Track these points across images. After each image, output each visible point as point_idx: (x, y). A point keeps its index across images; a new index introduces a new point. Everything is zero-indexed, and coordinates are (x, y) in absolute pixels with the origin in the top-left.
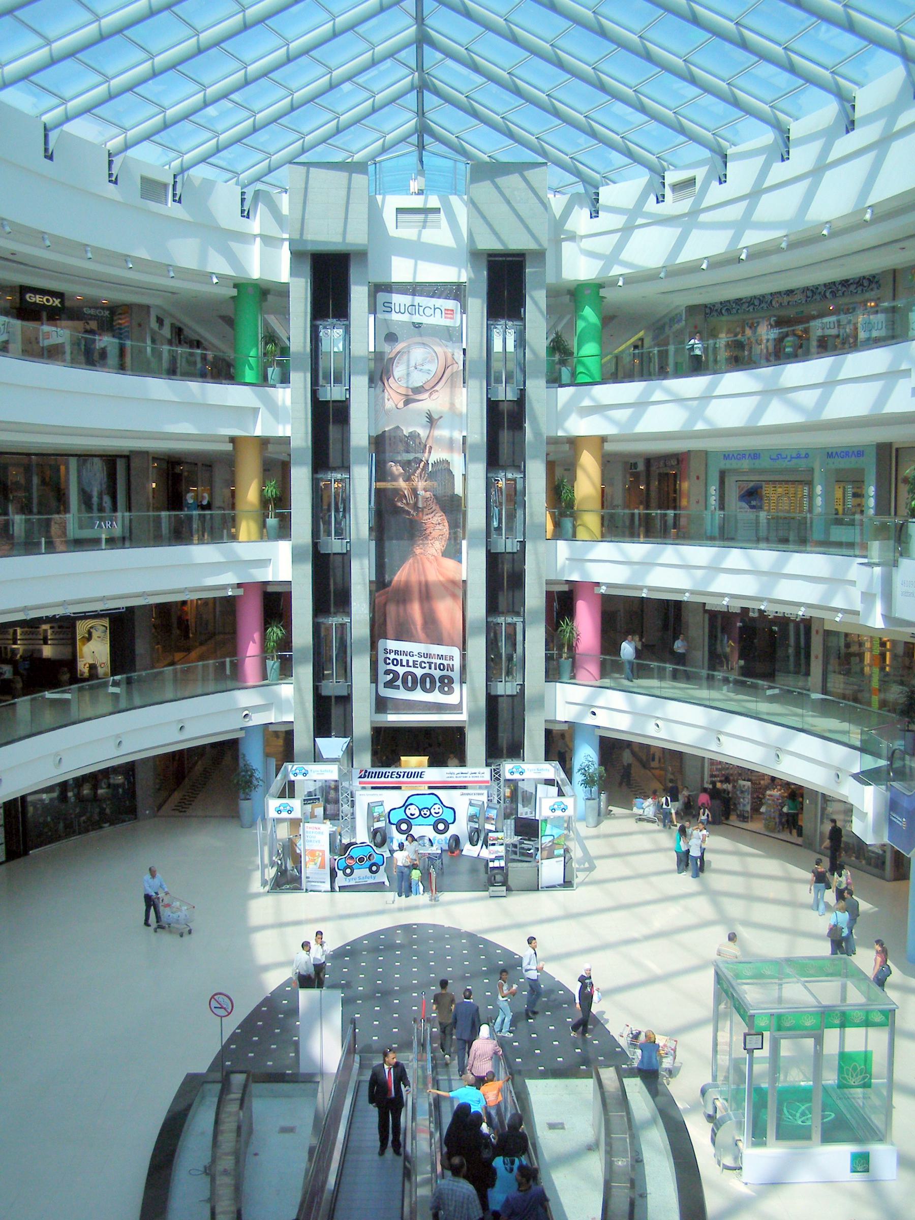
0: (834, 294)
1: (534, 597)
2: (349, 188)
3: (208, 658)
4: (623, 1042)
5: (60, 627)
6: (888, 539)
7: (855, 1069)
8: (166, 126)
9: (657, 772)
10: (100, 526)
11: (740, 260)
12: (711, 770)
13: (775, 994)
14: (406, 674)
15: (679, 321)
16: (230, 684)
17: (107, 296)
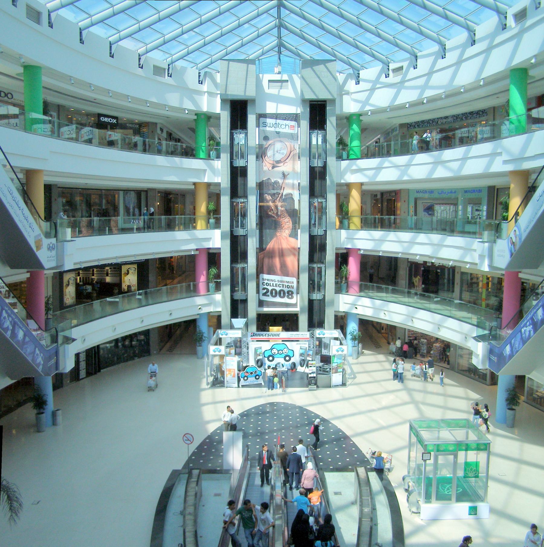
0: (466, 118)
1: (330, 256)
2: (247, 71)
3: (182, 282)
4: (368, 456)
5: (114, 268)
6: (492, 230)
7: (471, 469)
8: (165, 43)
9: (384, 335)
10: (133, 222)
11: (423, 103)
12: (409, 334)
13: (437, 435)
14: (272, 290)
15: (396, 130)
16: (193, 294)
17: (138, 118)
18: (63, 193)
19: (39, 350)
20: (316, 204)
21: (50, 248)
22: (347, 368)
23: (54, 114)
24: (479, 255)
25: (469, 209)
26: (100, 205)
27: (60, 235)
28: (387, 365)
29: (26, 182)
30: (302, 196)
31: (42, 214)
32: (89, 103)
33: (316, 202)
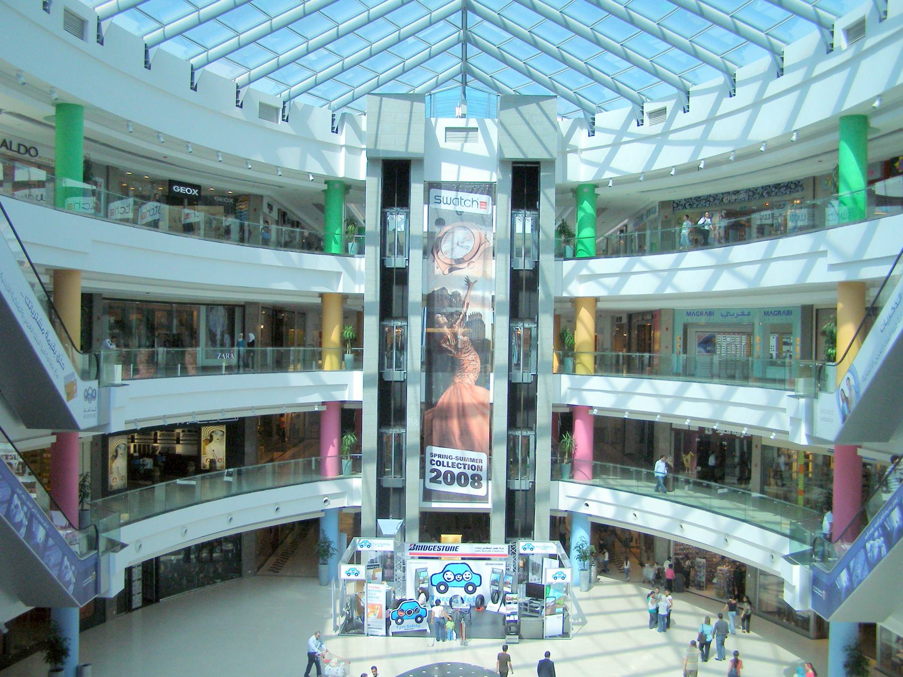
0: (769, 194)
1: (543, 417)
2: (411, 113)
5: (189, 431)
6: (810, 376)
8: (279, 67)
10: (221, 357)
11: (699, 169)
12: (675, 550)
14: (446, 473)
15: (655, 212)
16: (315, 477)
17: (233, 188)
18: (111, 307)
19: (69, 559)
20: (521, 331)
21: (88, 397)
22: (570, 605)
23: (101, 181)
24: (791, 418)
25: (773, 341)
26: (169, 327)
27: (104, 376)
28: (639, 602)
29: (54, 288)
30: (498, 318)
31: (78, 344)
32: (155, 162)
33: (520, 328)
